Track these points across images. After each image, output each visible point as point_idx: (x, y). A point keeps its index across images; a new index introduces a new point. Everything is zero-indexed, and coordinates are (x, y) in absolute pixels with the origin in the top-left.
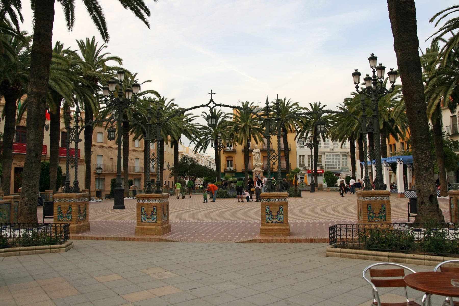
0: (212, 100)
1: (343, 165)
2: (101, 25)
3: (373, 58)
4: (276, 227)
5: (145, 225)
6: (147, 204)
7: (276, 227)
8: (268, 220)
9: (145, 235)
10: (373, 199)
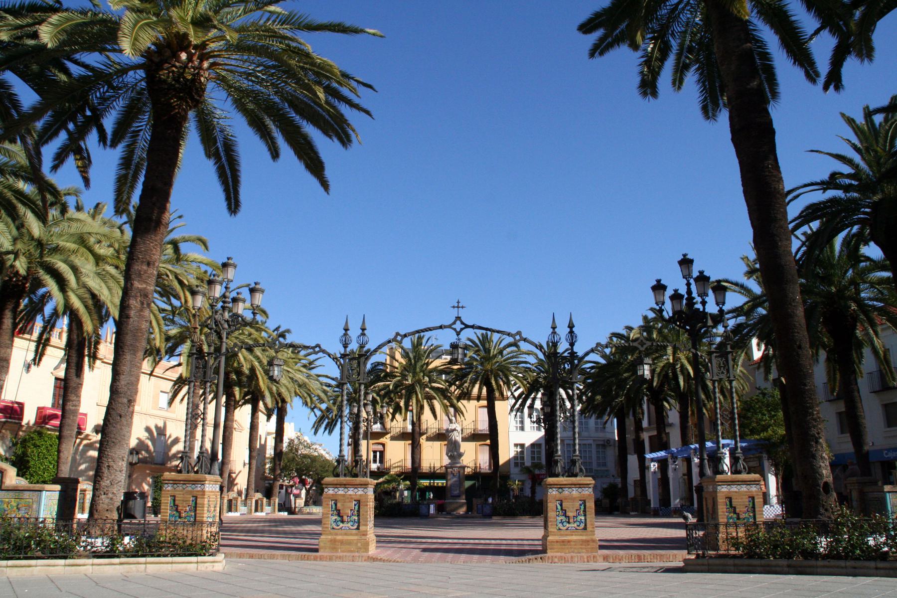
0: (458, 318)
1: (599, 465)
2: (231, 184)
3: (686, 262)
4: (574, 538)
5: (336, 534)
6: (344, 495)
7: (574, 538)
8: (560, 526)
9: (337, 551)
10: (734, 488)
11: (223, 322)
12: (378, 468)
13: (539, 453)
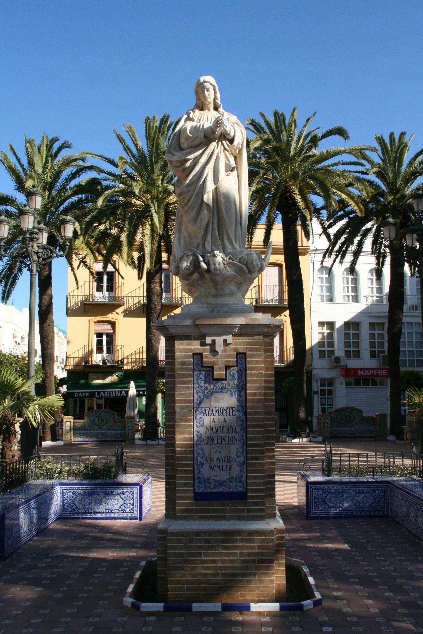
11: (33, 253)
12: (104, 361)
13: (357, 336)
